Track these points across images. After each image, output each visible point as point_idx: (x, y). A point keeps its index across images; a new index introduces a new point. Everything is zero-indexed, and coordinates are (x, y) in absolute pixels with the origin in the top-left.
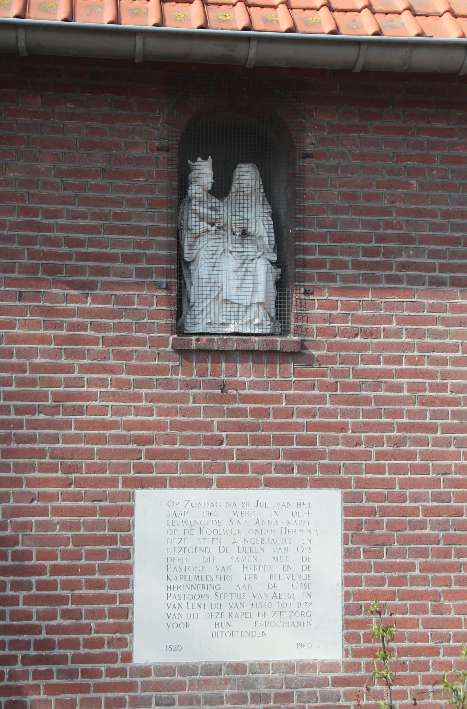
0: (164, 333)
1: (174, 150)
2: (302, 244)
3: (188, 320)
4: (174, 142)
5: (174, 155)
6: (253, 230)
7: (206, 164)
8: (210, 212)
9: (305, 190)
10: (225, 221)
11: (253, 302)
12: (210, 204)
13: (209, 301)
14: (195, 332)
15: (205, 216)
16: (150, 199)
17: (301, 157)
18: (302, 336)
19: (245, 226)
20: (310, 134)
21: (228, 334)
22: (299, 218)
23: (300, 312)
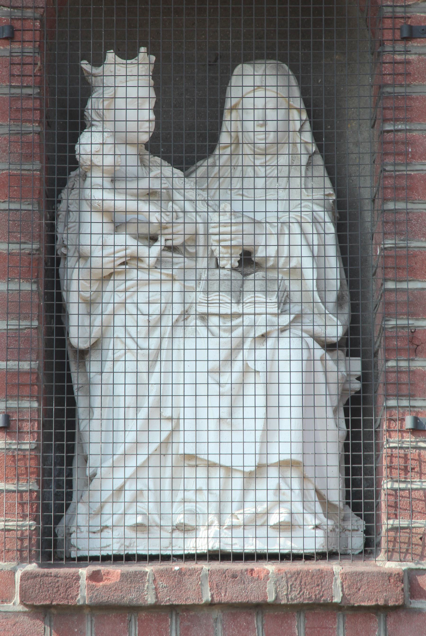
1: (28, 36)
2: (404, 285)
3: (81, 520)
4: (29, 13)
5: (29, 48)
6: (272, 251)
7: (133, 69)
8: (144, 206)
9: (410, 130)
10: (190, 229)
12: (144, 184)
13: (132, 462)
14: (104, 553)
15: (130, 217)
17: (398, 36)
18: (409, 557)
19: (248, 241)
21: (189, 557)
22: (396, 211)
23: (403, 486)
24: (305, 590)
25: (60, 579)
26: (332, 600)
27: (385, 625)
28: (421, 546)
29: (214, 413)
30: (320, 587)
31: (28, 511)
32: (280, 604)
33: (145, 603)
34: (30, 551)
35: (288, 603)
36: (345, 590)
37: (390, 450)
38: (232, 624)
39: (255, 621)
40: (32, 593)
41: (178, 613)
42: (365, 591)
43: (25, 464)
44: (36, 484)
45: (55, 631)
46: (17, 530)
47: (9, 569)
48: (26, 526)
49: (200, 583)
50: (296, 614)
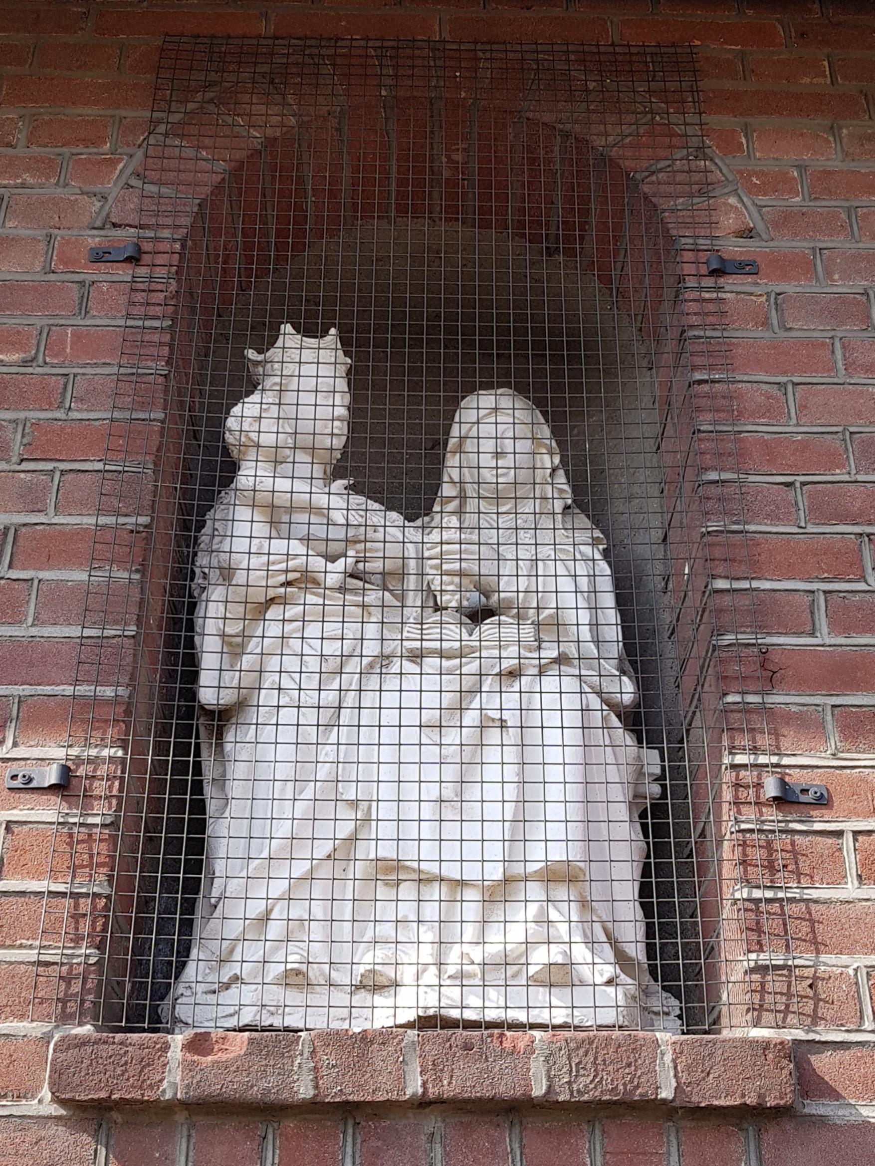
0: (22, 1017)
1: (161, 259)
11: (518, 869)
13: (301, 868)
16: (36, 425)
18: (792, 1019)
20: (732, 200)
24: (604, 1073)
25: (130, 1049)
26: (657, 1094)
27: (759, 1148)
28: (811, 998)
29: (431, 791)
30: (633, 1068)
31: (85, 927)
32: (557, 1102)
33: (293, 1098)
34: (83, 1001)
35: (573, 1100)
36: (680, 1075)
37: (740, 834)
38: (462, 1144)
39: (508, 1140)
40: (74, 1075)
41: (359, 1124)
42: (719, 1076)
43: (90, 849)
44: (106, 883)
45: (116, 1157)
46: (62, 964)
47: (39, 1035)
48: (80, 956)
49: (401, 1059)
50: (585, 1126)
